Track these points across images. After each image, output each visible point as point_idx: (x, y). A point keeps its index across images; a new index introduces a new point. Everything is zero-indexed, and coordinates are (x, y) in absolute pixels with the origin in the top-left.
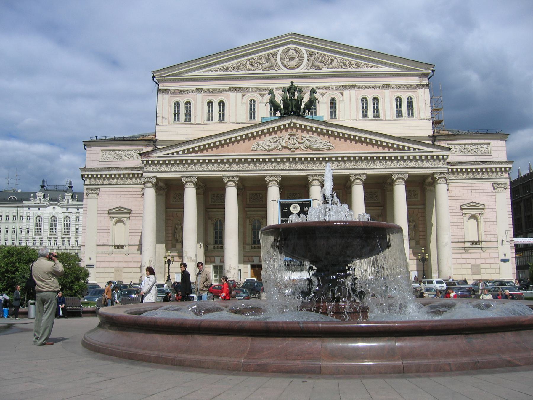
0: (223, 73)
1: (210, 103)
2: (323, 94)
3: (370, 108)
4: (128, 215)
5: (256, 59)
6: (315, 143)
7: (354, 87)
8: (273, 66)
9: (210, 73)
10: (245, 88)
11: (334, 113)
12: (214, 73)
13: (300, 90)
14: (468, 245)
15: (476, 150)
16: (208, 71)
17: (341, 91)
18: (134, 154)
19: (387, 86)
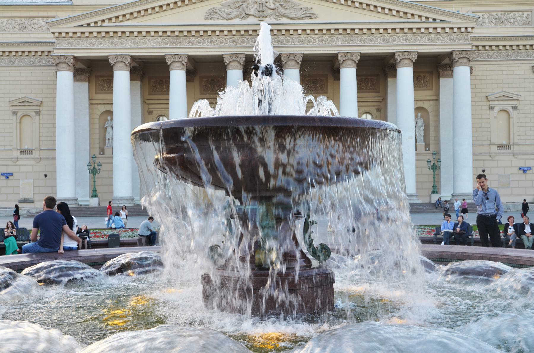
4: (37, 108)
6: (292, 10)
14: (494, 149)
15: (512, 21)
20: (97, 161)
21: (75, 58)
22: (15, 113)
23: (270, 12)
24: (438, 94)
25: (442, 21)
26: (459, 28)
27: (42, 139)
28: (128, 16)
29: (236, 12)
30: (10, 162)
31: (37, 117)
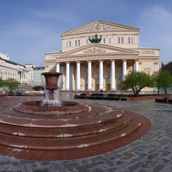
1: (76, 41)
3: (121, 40)
7: (116, 34)
11: (110, 42)
12: (77, 33)
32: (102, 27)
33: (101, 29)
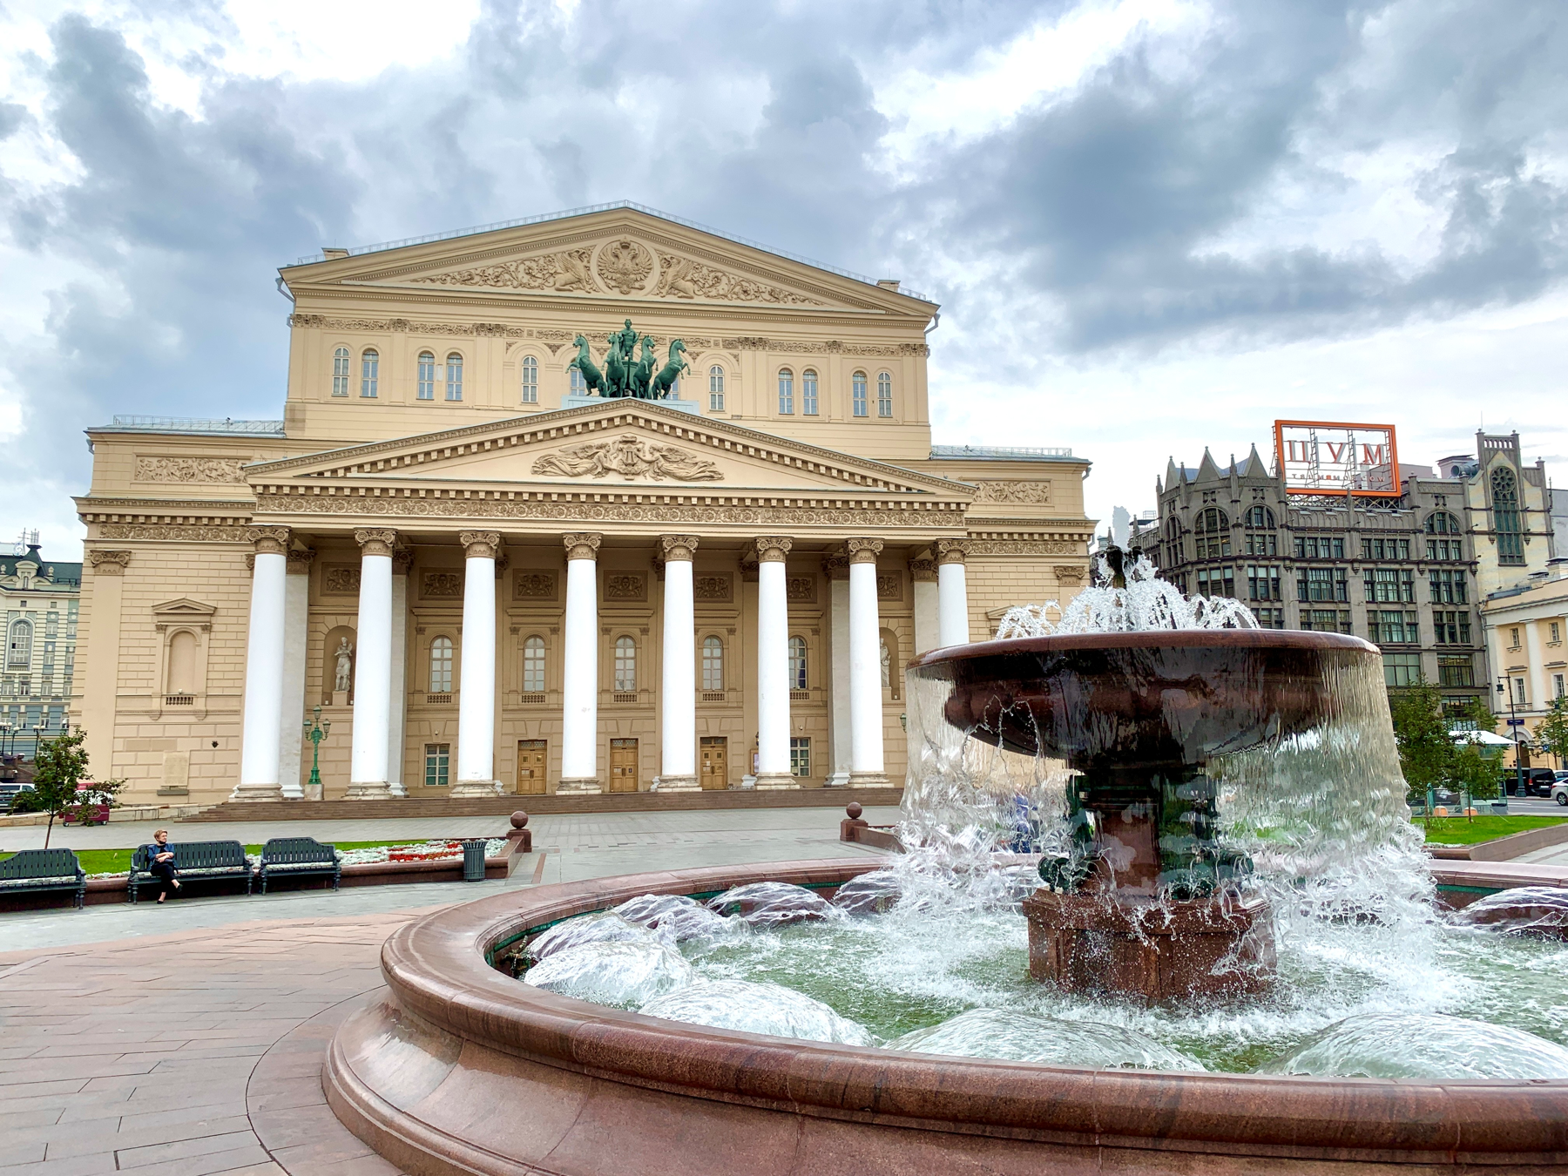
0: (459, 287)
2: (695, 356)
4: (207, 618)
5: (541, 262)
8: (579, 281)
9: (428, 285)
10: (850, 346)
11: (717, 400)
12: (438, 285)
13: (649, 344)
16: (424, 279)
17: (735, 352)
18: (227, 468)
19: (400, 324)
20: (323, 717)
21: (291, 530)
22: (161, 628)
23: (644, 466)
24: (911, 607)
25: (920, 492)
26: (948, 504)
27: (211, 675)
28: (394, 463)
29: (587, 464)
30: (146, 719)
31: (206, 637)
32: (657, 269)
33: (648, 292)
